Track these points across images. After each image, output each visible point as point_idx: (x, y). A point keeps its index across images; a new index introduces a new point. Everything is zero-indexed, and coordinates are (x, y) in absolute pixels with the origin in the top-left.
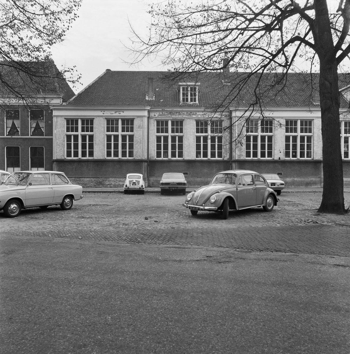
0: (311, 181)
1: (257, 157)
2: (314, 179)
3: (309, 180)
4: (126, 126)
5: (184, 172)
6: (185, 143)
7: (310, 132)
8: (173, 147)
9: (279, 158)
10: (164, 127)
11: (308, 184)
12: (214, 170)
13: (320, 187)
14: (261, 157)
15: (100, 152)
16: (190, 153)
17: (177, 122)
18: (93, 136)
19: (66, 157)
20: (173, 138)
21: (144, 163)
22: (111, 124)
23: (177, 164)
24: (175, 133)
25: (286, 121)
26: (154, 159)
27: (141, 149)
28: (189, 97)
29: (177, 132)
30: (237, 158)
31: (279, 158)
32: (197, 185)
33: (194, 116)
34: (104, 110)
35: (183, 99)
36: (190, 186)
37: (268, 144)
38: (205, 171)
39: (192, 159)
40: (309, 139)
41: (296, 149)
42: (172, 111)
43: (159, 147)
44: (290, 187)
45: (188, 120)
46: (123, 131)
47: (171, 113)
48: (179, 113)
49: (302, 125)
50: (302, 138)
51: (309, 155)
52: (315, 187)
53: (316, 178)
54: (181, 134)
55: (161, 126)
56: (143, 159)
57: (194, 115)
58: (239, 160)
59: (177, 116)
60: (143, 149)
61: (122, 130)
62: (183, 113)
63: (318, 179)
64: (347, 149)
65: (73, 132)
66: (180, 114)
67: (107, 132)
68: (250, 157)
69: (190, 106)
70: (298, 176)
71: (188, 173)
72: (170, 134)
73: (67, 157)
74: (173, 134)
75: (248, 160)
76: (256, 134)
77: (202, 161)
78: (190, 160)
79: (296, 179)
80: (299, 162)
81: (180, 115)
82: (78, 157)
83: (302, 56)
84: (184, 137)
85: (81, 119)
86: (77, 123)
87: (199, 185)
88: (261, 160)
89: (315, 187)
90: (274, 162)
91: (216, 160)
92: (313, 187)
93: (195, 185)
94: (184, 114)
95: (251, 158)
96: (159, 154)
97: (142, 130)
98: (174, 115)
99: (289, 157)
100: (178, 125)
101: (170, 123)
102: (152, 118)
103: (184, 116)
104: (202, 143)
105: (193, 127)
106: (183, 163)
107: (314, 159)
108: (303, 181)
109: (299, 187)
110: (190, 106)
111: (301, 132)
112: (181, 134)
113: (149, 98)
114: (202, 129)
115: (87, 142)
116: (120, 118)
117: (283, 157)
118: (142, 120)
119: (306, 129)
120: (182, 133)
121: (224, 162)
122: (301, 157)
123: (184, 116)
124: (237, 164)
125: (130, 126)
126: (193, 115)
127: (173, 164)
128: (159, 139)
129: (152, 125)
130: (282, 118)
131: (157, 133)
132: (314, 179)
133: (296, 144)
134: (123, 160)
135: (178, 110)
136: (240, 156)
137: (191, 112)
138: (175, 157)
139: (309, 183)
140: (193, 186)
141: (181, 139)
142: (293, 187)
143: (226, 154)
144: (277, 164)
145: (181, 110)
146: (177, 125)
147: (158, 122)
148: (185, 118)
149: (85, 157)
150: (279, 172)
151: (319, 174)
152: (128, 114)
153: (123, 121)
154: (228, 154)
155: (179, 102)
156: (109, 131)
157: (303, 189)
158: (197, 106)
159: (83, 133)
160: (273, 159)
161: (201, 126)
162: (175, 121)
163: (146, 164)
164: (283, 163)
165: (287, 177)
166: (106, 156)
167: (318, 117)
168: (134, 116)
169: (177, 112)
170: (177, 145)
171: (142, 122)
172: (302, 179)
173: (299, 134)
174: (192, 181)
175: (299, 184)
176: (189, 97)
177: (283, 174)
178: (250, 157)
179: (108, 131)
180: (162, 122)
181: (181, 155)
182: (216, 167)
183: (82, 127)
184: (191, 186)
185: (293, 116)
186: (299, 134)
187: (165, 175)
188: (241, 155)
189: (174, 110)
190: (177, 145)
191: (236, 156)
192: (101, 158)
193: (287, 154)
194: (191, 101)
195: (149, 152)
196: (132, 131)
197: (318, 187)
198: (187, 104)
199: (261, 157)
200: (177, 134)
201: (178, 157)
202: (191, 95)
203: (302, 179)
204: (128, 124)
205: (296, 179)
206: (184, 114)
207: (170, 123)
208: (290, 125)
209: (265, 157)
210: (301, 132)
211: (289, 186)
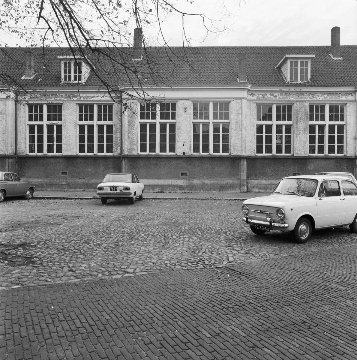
0: (227, 184)
1: (271, 153)
2: (231, 181)
3: (225, 182)
4: (84, 113)
5: (63, 171)
6: (64, 134)
7: (342, 119)
8: (50, 139)
9: (184, 153)
10: (38, 113)
11: (222, 188)
12: (101, 169)
13: (239, 191)
14: (276, 153)
15: (71, 146)
16: (71, 146)
17: (55, 107)
18: (62, 126)
19: (28, 152)
20: (50, 128)
21: (7, 159)
22: (200, 109)
23: (53, 160)
24: (52, 121)
25: (310, 106)
26: (25, 154)
27: (4, 141)
28: (72, 75)
29: (55, 120)
30: (126, 153)
31: (184, 153)
32: (78, 188)
33: (75, 99)
34: (336, 93)
35: (65, 77)
36: (69, 190)
37: (169, 134)
38: (90, 169)
39: (73, 154)
40: (341, 129)
41: (154, 140)
42: (46, 93)
43: (32, 139)
44: (198, 192)
45: (68, 104)
46: (215, 118)
47: (45, 94)
48: (55, 94)
49: (49, 110)
50: (332, 128)
51: (226, 149)
52: (232, 192)
53: (234, 180)
54: (59, 123)
55: (35, 112)
56: (7, 154)
57: (75, 97)
58: (129, 155)
59: (53, 99)
60: (7, 142)
61: (277, 119)
62: (61, 94)
63: (236, 182)
64: (280, 142)
65: (144, 119)
66: (57, 97)
67: (79, 120)
68: (146, 151)
69: (73, 86)
70: (210, 177)
71: (67, 172)
72: (45, 122)
73: (140, 152)
74: (49, 123)
75: (100, 156)
76: (40, 123)
77: (86, 158)
78: (69, 156)
79: (206, 181)
80: (212, 159)
81: (57, 98)
82: (43, 152)
83: (127, 22)
84: (176, 125)
85: (97, 104)
86: (92, 110)
87: (81, 188)
88: (161, 155)
89: (232, 192)
90: (178, 158)
91: (336, 156)
92: (229, 192)
93: (75, 188)
94: (62, 96)
95: (147, 153)
96: (32, 150)
97: (5, 116)
98: (49, 97)
99: (199, 152)
100: (56, 111)
101: (45, 108)
102: (21, 102)
103: (62, 99)
104: (86, 134)
105: (74, 113)
106: (61, 160)
107: (232, 154)
108: (216, 184)
109: (210, 192)
110: (73, 86)
111: (161, 119)
112: (59, 123)
113: (26, 77)
114: (168, 114)
115: (317, 134)
116: (274, 103)
117: (190, 152)
118: (5, 105)
119: (168, 114)
120: (112, 120)
121: (113, 158)
122: (329, 152)
123: (62, 99)
124: (126, 161)
125: (171, 111)
126: (74, 97)
127: (48, 160)
128: (32, 129)
129: (22, 111)
130: (187, 99)
131: (79, 121)
132: (231, 181)
133: (208, 134)
134: (81, 156)
135: (53, 91)
136: (131, 150)
137: (71, 93)
138: (262, 153)
139: (225, 186)
140: (73, 190)
141: (60, 128)
142: (202, 191)
143: (117, 148)
144: (180, 162)
145: (57, 91)
146: (55, 111)
147: (30, 107)
148: (63, 101)
149: (32, 153)
150: (184, 172)
151: (238, 175)
152: (168, 95)
153: (215, 103)
154: (119, 148)
155: (61, 81)
156: (217, 119)
157: (216, 194)
158: (287, 85)
159: (332, 123)
160: (293, 155)
161: (85, 111)
162: (52, 105)
163: (11, 160)
164: (190, 159)
165: (194, 178)
166: (139, 151)
167: (351, 101)
168: (230, 98)
169: (53, 93)
170: (55, 136)
171: (4, 107)
172: (215, 181)
173: (327, 122)
174: (71, 183)
175: (211, 188)
176: (72, 75)
177: (188, 174)
178: (146, 151)
179: (81, 119)
180: (36, 107)
181: (59, 149)
182: (103, 166)
183: (214, 113)
184: (71, 190)
185: (211, 97)
186: (158, 121)
187: (108, 177)
188: (132, 149)
189: (48, 91)
190: (55, 136)
191: (126, 150)
192: (74, 154)
193: (196, 148)
194: (75, 79)
195: (19, 146)
196: (174, 117)
197: (237, 192)
198: (69, 83)
199: (276, 153)
200: (54, 122)
201: (285, 153)
202: (75, 72)
203: (215, 181)
204: (55, 111)
205: (206, 181)
206: (62, 96)
207: (45, 108)
208: (316, 110)
209: (314, 152)
210: (277, 120)
211: (196, 190)
